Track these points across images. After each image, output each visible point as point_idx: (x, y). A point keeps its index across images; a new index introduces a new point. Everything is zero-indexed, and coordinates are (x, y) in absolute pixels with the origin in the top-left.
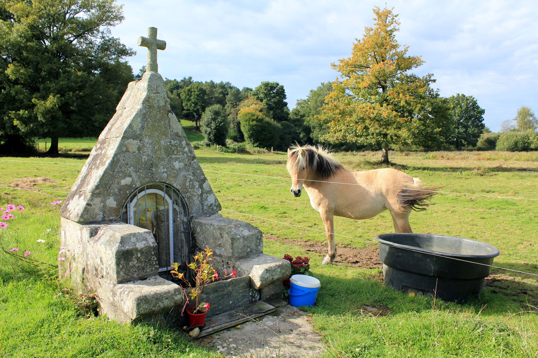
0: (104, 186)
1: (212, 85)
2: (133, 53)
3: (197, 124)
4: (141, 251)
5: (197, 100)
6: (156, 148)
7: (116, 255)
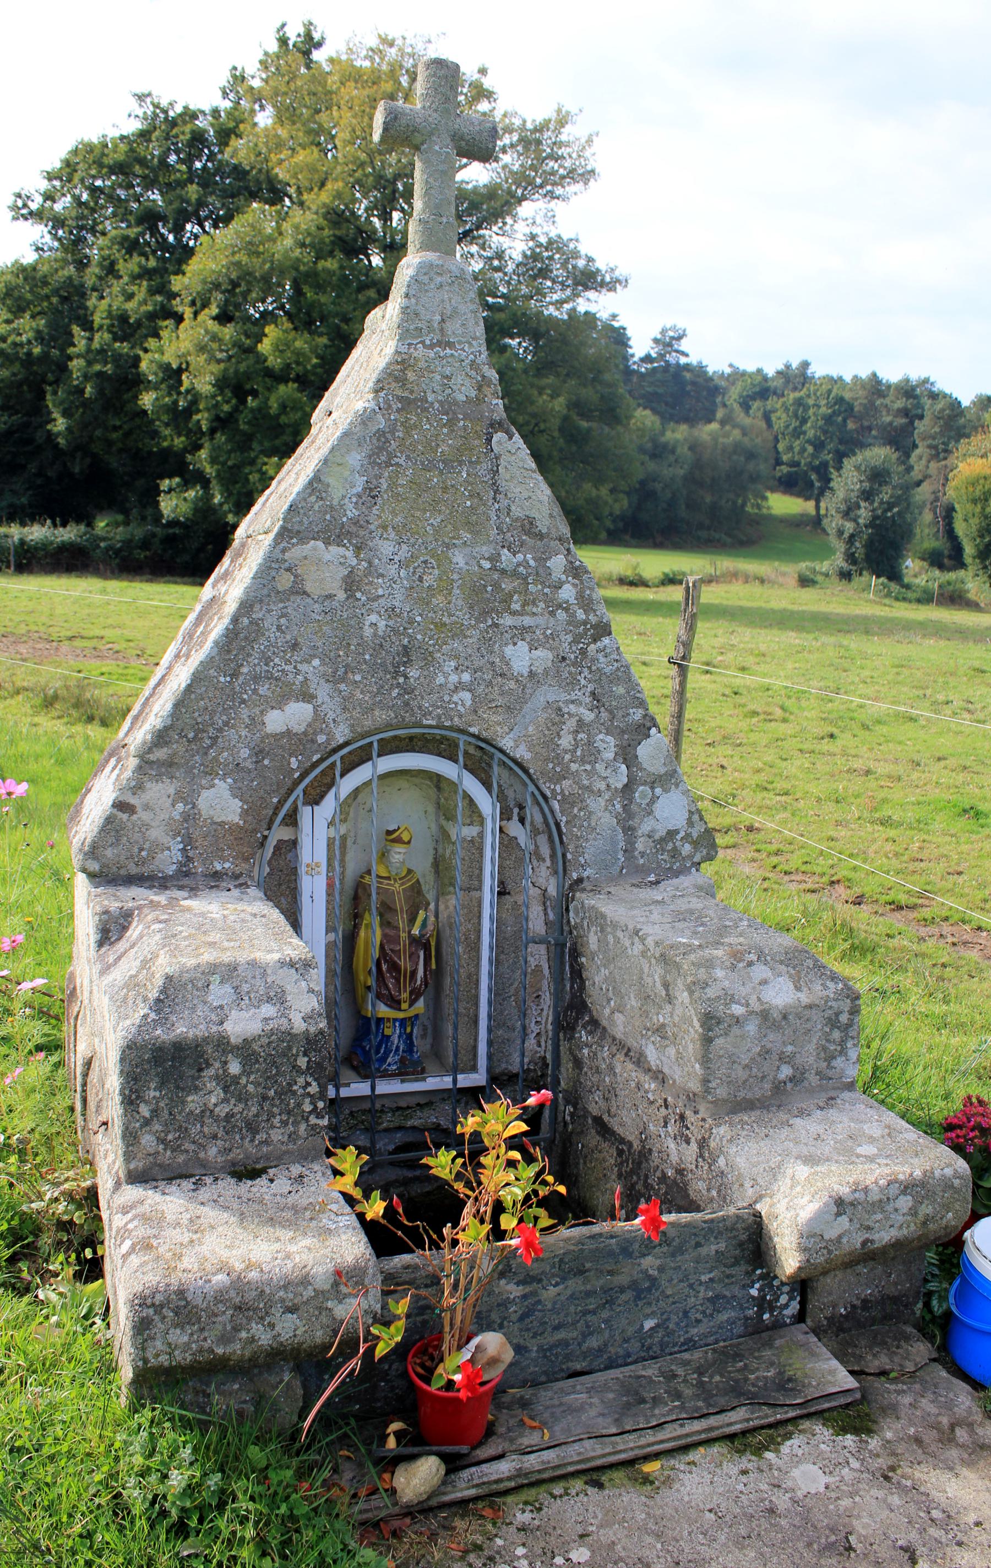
0: (191, 735)
1: (875, 387)
2: (618, 281)
3: (817, 508)
4: (246, 1050)
5: (825, 432)
6: (429, 580)
7: (122, 1060)
